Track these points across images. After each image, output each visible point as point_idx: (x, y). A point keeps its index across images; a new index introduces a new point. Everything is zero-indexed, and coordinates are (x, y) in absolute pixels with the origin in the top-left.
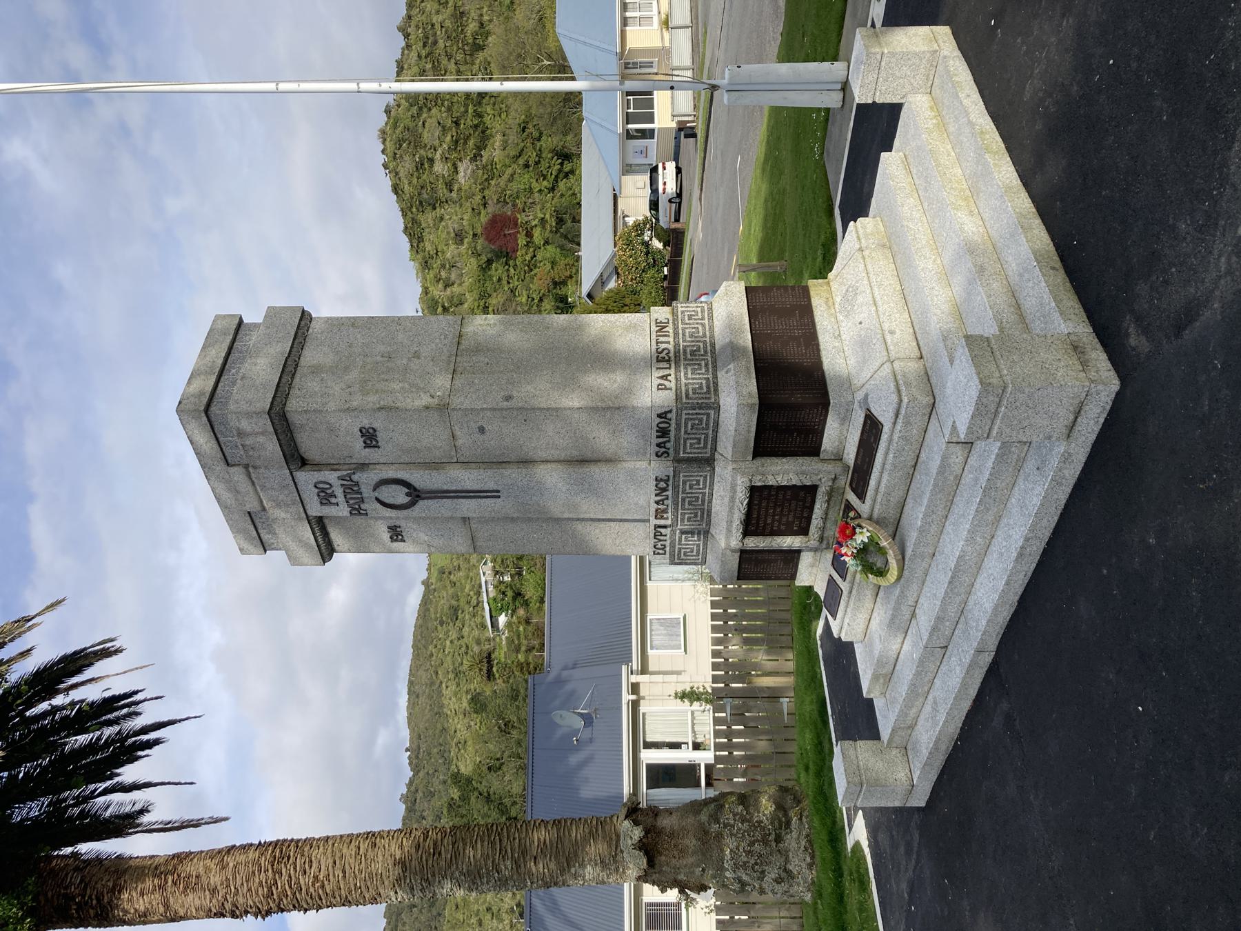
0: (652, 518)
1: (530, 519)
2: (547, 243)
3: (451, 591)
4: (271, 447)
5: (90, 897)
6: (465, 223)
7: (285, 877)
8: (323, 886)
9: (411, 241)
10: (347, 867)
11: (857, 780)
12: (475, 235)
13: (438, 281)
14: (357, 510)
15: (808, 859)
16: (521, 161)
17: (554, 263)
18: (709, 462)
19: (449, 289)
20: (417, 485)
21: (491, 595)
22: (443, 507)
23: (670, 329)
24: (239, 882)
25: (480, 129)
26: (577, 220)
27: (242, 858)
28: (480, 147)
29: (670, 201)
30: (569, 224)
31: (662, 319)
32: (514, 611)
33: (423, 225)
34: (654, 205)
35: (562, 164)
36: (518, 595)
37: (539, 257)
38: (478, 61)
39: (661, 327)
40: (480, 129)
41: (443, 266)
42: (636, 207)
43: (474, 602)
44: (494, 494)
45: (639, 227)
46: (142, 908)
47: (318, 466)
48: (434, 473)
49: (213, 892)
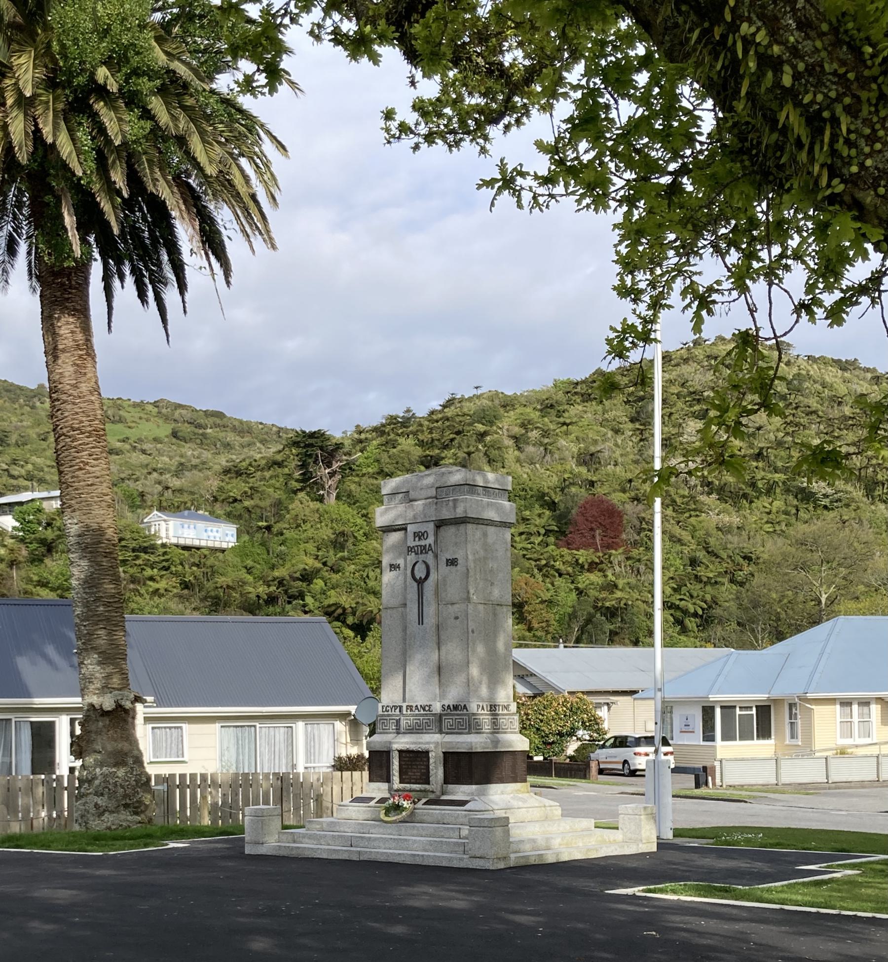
0: (407, 704)
1: (405, 640)
2: (580, 592)
3: (33, 433)
4: (446, 514)
5: (70, 293)
6: (610, 468)
7: (87, 440)
8: (81, 469)
9: (583, 382)
10: (95, 487)
11: (265, 814)
12: (592, 484)
13: (523, 425)
14: (410, 550)
15: (113, 827)
16: (701, 555)
17: (550, 603)
18: (441, 732)
19: (510, 442)
20: (426, 583)
21: (45, 505)
22: (412, 595)
23: (505, 712)
24: (82, 405)
25: (749, 490)
26: (613, 638)
27: (97, 406)
28: (723, 493)
29: (625, 762)
30: (608, 627)
31: (510, 708)
32: (22, 540)
33: (607, 403)
34: (621, 742)
35: (695, 615)
36: (49, 547)
37: (558, 581)
38: (849, 488)
39: (506, 707)
40: (749, 490)
41: (546, 433)
42: (618, 719)
43: (16, 471)
44: (421, 620)
45: (593, 723)
46: (62, 332)
47: (436, 535)
48: (433, 592)
49: (75, 387)
